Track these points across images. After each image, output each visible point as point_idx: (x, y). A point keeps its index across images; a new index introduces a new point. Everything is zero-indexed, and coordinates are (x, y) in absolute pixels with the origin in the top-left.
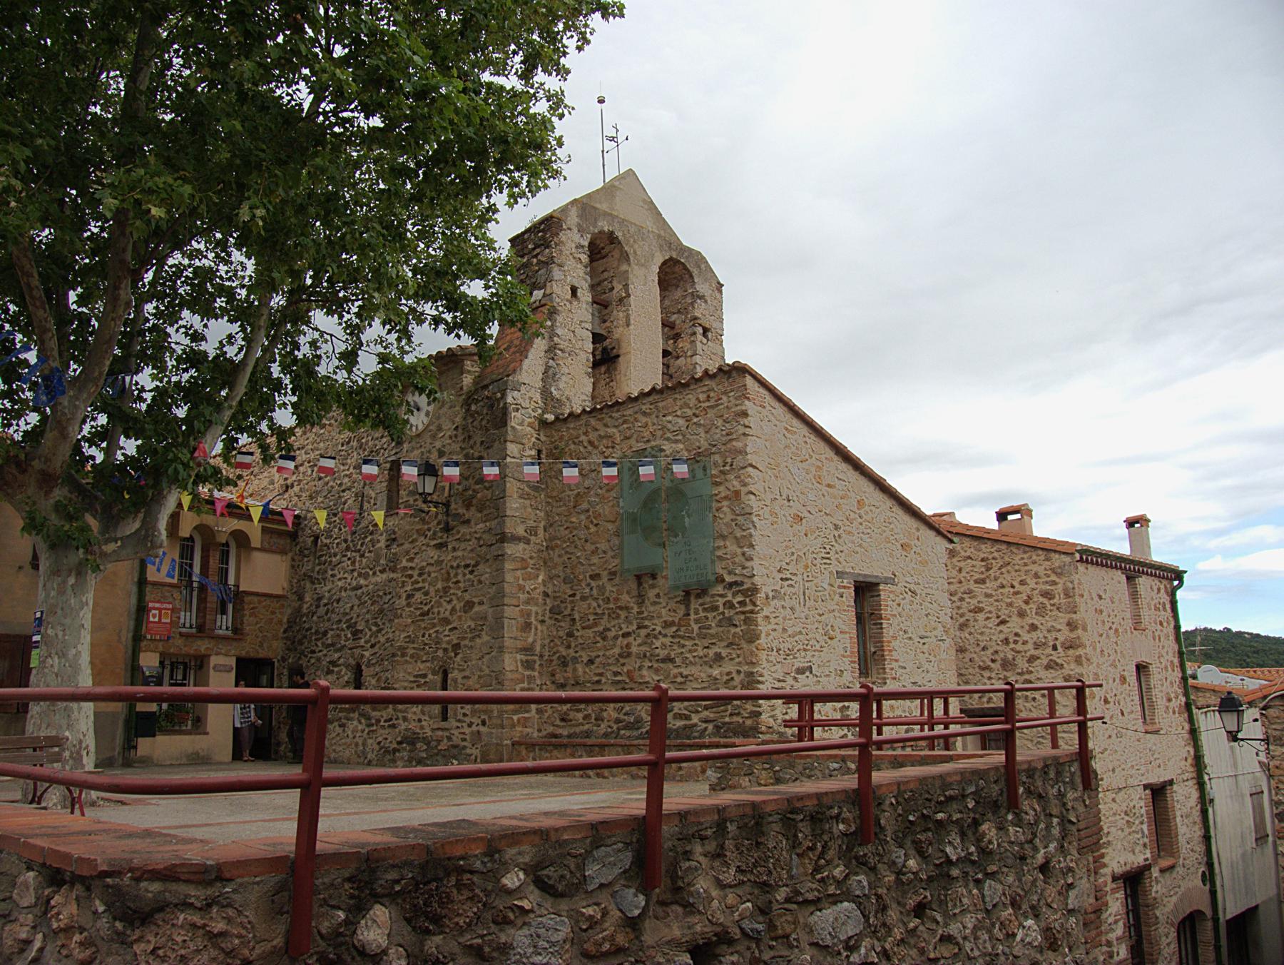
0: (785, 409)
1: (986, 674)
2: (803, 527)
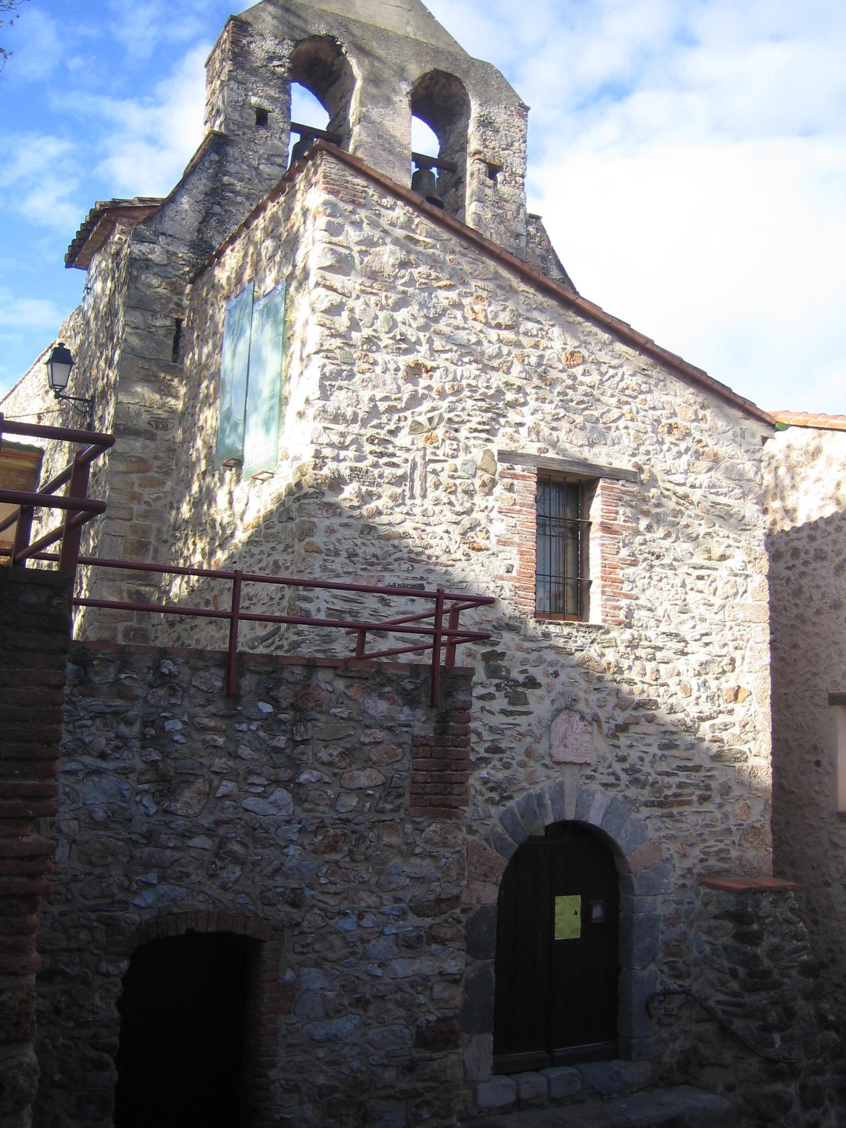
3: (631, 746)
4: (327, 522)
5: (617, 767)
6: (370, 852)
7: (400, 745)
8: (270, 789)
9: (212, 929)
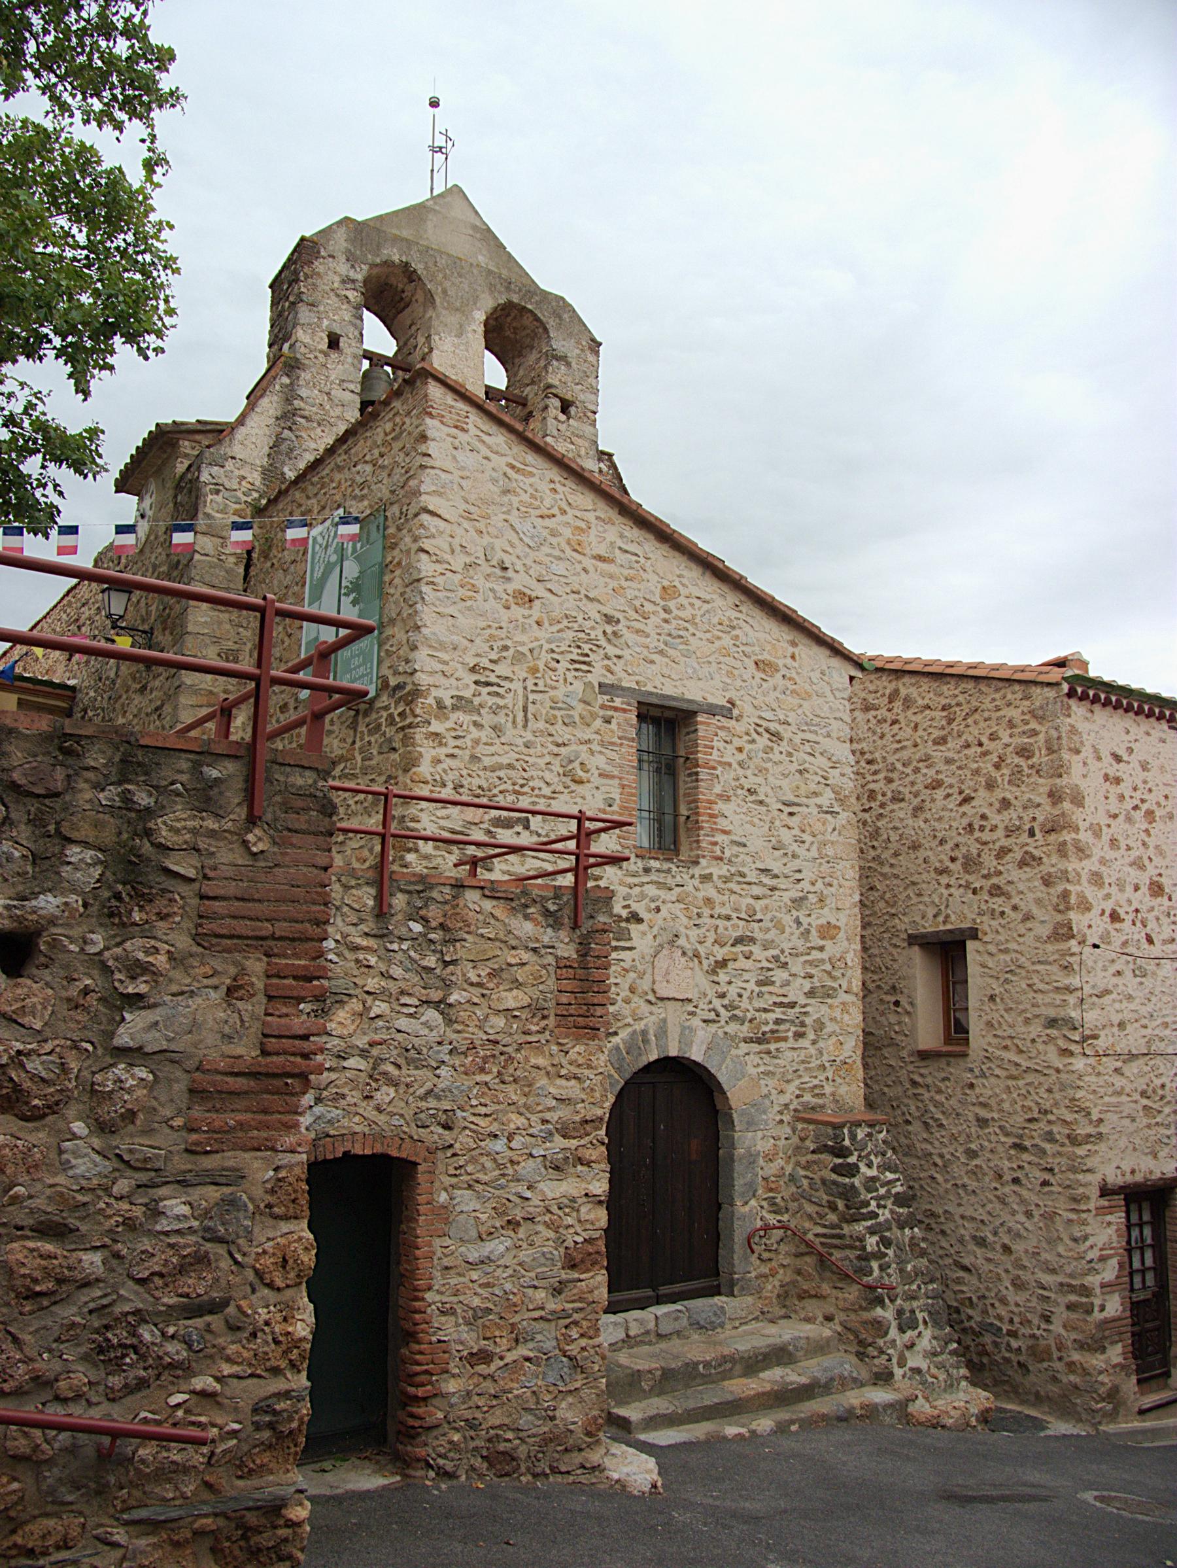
0: (513, 437)
1: (944, 880)
2: (536, 611)
3: (730, 983)
4: (434, 752)
5: (717, 1003)
6: (518, 1073)
7: (544, 967)
8: (421, 1010)
9: (368, 1152)
